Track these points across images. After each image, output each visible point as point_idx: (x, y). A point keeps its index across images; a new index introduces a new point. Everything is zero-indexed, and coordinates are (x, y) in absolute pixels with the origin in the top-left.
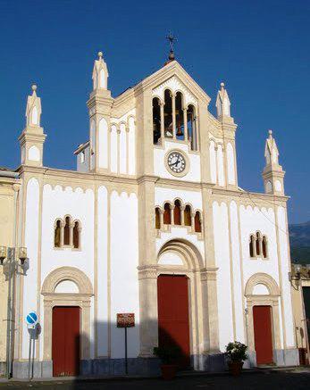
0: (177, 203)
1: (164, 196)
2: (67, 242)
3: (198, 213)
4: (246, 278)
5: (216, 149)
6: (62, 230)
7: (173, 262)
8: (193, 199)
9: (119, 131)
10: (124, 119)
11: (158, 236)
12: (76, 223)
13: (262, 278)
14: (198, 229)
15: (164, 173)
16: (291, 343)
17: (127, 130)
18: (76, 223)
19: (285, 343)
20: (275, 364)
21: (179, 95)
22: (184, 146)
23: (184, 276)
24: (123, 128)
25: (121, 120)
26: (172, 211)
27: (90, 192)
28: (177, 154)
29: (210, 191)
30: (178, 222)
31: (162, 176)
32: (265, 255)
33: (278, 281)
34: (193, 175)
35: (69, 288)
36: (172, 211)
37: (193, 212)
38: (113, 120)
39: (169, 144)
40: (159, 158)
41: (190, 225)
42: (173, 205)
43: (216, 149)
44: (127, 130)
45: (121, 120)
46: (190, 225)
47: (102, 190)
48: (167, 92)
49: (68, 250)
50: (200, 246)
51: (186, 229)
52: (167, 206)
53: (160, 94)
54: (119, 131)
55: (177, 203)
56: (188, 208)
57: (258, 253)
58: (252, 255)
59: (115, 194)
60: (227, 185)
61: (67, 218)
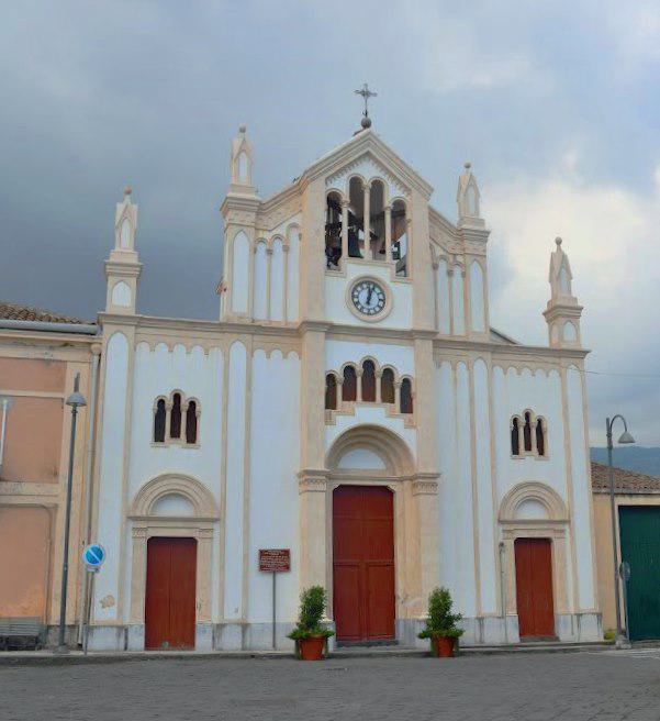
0: (369, 365)
1: (350, 353)
2: (175, 434)
3: (406, 382)
4: (504, 491)
5: (450, 273)
6: (521, 431)
7: (365, 467)
8: (400, 360)
9: (270, 252)
10: (281, 231)
11: (329, 421)
12: (540, 421)
13: (533, 493)
14: (407, 407)
15: (343, 316)
16: (588, 602)
17: (286, 249)
18: (540, 421)
19: (576, 600)
20: (557, 639)
21: (378, 187)
22: (384, 272)
23: (385, 488)
24: (278, 246)
25: (275, 232)
26: (359, 380)
27: (217, 353)
28: (371, 284)
29: (429, 345)
30: (369, 396)
31: (337, 321)
32: (541, 451)
33: (565, 498)
34: (401, 315)
35: (532, 513)
36: (359, 380)
37: (398, 380)
38: (261, 234)
39: (352, 269)
40: (335, 297)
41: (393, 402)
42: (359, 369)
43: (450, 273)
44: (286, 249)
45: (275, 232)
46: (393, 402)
47: (238, 350)
48: (355, 184)
49: (529, 459)
50: (409, 437)
51: (383, 410)
52: (349, 370)
53: (342, 186)
54: (270, 252)
55: (369, 365)
56: (389, 373)
57: (528, 447)
58: (515, 451)
59: (144, 347)
60: (451, 335)
61: (527, 416)
